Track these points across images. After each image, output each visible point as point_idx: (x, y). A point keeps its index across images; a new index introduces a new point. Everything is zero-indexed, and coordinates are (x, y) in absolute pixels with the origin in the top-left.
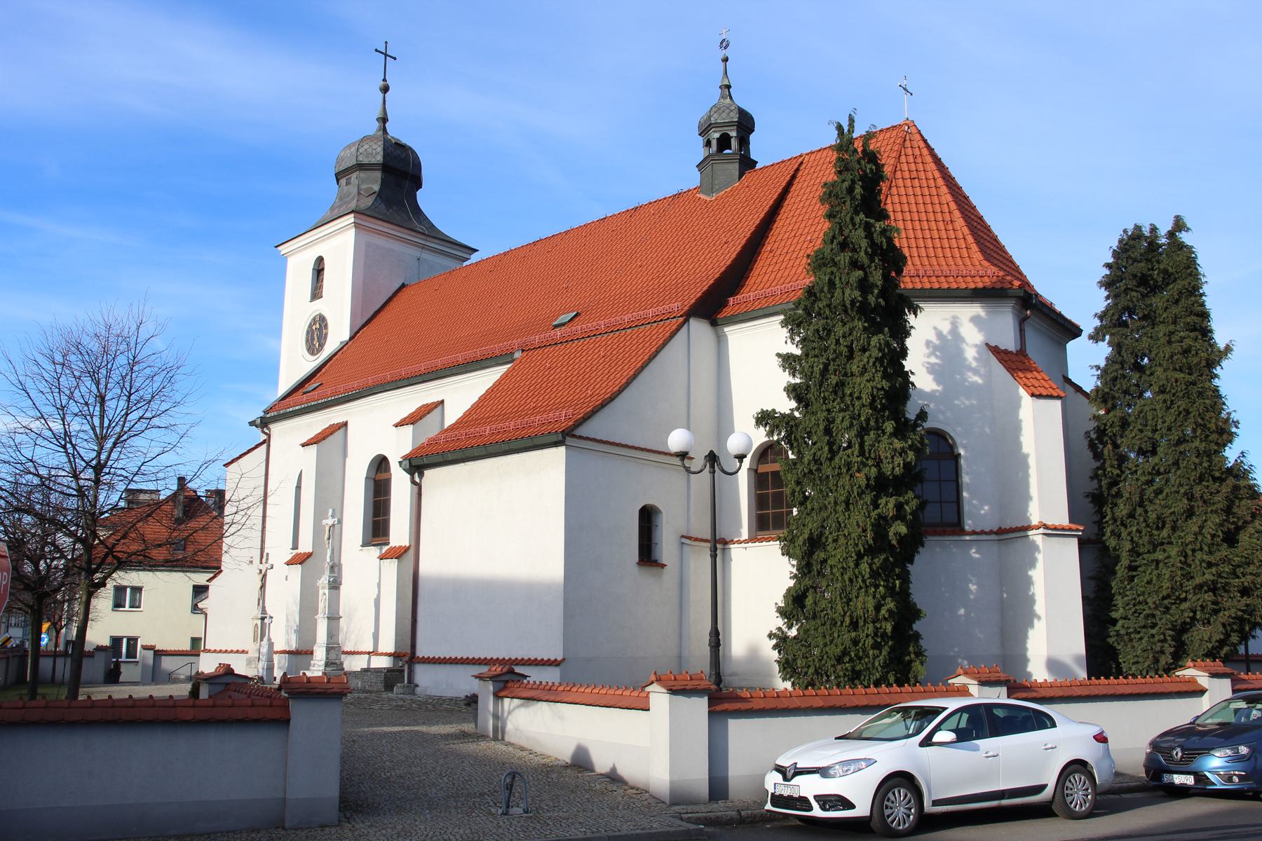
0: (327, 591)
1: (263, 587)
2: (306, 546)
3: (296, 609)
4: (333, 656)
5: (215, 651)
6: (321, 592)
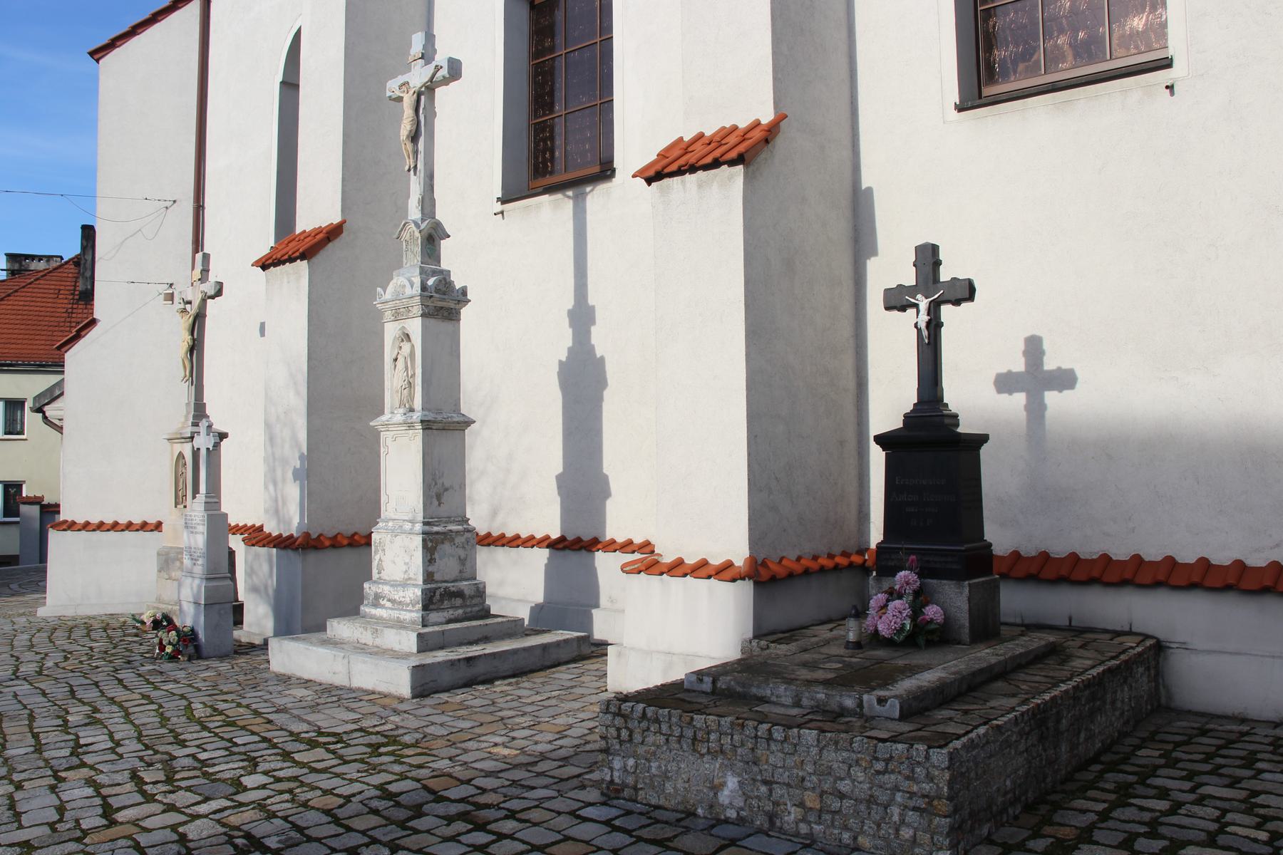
0: (415, 326)
1: (196, 348)
2: (319, 206)
3: (295, 402)
4: (447, 567)
5: (86, 526)
6: (391, 331)
